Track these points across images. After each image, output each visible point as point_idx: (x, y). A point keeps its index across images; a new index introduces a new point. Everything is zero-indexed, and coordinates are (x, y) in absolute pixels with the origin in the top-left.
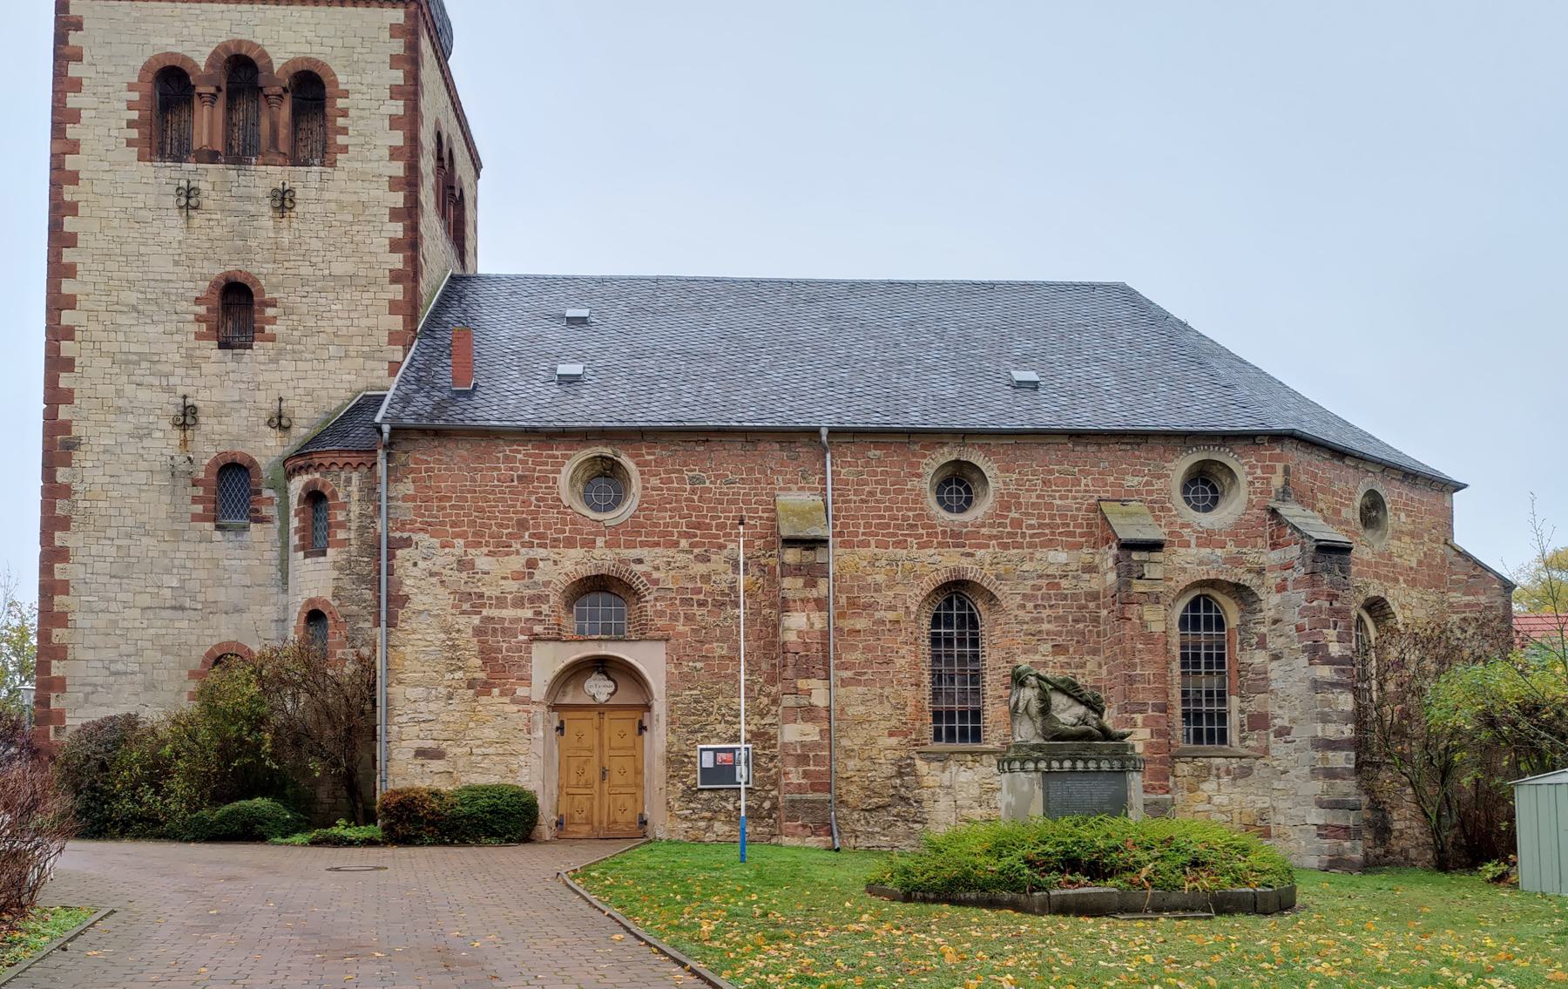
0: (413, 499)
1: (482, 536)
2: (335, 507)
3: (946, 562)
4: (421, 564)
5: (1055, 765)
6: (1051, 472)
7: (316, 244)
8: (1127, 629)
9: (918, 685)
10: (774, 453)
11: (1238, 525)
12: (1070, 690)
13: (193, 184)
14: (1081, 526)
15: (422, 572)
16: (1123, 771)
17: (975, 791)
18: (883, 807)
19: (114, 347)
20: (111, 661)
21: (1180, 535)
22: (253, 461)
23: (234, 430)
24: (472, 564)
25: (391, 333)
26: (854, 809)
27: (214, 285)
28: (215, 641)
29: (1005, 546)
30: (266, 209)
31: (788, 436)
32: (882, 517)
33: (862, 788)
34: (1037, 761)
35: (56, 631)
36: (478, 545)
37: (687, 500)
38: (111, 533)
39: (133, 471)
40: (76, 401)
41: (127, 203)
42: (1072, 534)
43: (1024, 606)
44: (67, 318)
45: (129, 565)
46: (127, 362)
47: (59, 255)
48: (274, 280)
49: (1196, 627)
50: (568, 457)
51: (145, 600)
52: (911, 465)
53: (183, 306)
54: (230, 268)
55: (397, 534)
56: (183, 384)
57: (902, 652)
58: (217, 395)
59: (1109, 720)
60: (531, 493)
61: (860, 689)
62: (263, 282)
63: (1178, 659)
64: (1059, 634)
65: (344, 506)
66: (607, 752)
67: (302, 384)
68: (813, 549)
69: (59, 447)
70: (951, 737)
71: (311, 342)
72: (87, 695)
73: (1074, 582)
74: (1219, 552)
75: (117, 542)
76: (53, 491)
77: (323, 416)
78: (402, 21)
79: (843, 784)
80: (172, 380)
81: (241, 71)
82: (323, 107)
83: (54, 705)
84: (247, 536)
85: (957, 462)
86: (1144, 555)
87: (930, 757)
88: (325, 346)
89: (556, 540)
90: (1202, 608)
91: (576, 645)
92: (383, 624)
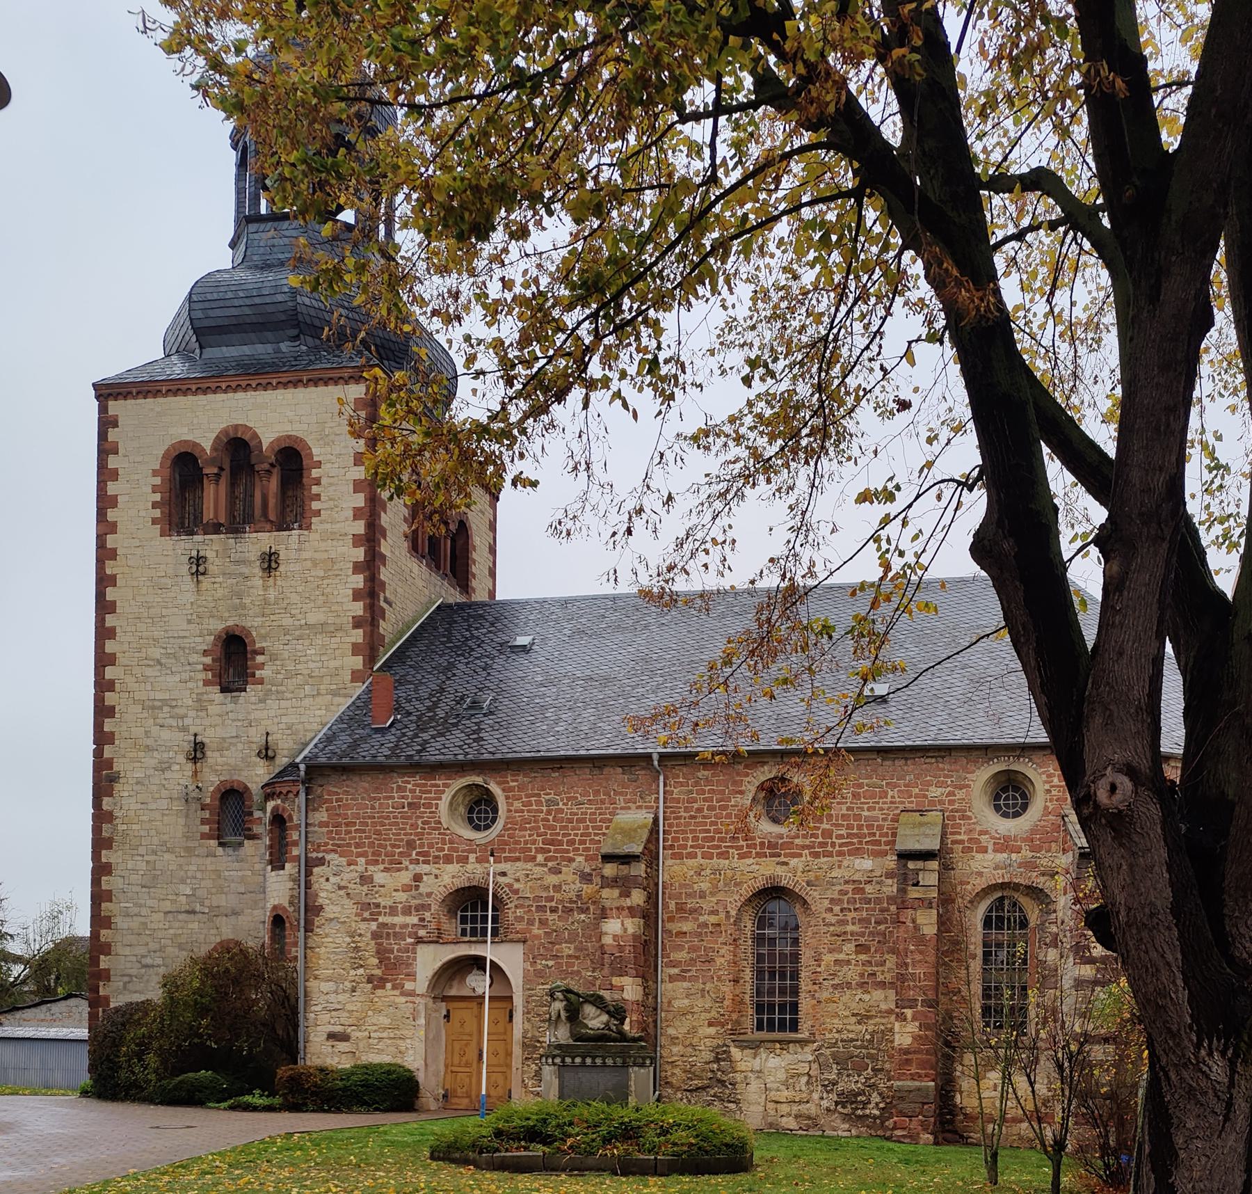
0: (326, 824)
1: (379, 855)
3: (762, 870)
4: (332, 879)
5: (568, 1060)
6: (861, 786)
7: (295, 598)
8: (901, 933)
9: (736, 981)
11: (1033, 831)
13: (201, 554)
15: (330, 885)
16: (625, 1066)
17: (782, 1076)
18: (704, 1088)
20: (143, 956)
21: (978, 841)
22: (246, 788)
23: (232, 761)
25: (353, 672)
26: (678, 1089)
27: (218, 638)
29: (816, 855)
30: (257, 571)
32: (708, 831)
33: (685, 1071)
34: (554, 1057)
35: (103, 932)
36: (376, 862)
37: (543, 820)
39: (159, 801)
40: (117, 742)
42: (878, 843)
43: (831, 910)
45: (155, 877)
47: (103, 620)
48: (263, 631)
51: (167, 906)
52: (735, 783)
53: (195, 658)
54: (230, 623)
55: (314, 855)
57: (722, 952)
58: (220, 732)
60: (418, 817)
61: (686, 984)
62: (254, 634)
64: (863, 934)
67: (284, 719)
68: (628, 863)
69: (105, 780)
70: (771, 1028)
72: (125, 984)
73: (878, 887)
74: (1014, 856)
75: (146, 858)
76: (101, 817)
79: (668, 1067)
80: (187, 721)
81: (238, 447)
82: (301, 476)
86: (920, 864)
87: (743, 1045)
88: (301, 686)
90: (1008, 907)
91: (452, 946)
92: (302, 930)
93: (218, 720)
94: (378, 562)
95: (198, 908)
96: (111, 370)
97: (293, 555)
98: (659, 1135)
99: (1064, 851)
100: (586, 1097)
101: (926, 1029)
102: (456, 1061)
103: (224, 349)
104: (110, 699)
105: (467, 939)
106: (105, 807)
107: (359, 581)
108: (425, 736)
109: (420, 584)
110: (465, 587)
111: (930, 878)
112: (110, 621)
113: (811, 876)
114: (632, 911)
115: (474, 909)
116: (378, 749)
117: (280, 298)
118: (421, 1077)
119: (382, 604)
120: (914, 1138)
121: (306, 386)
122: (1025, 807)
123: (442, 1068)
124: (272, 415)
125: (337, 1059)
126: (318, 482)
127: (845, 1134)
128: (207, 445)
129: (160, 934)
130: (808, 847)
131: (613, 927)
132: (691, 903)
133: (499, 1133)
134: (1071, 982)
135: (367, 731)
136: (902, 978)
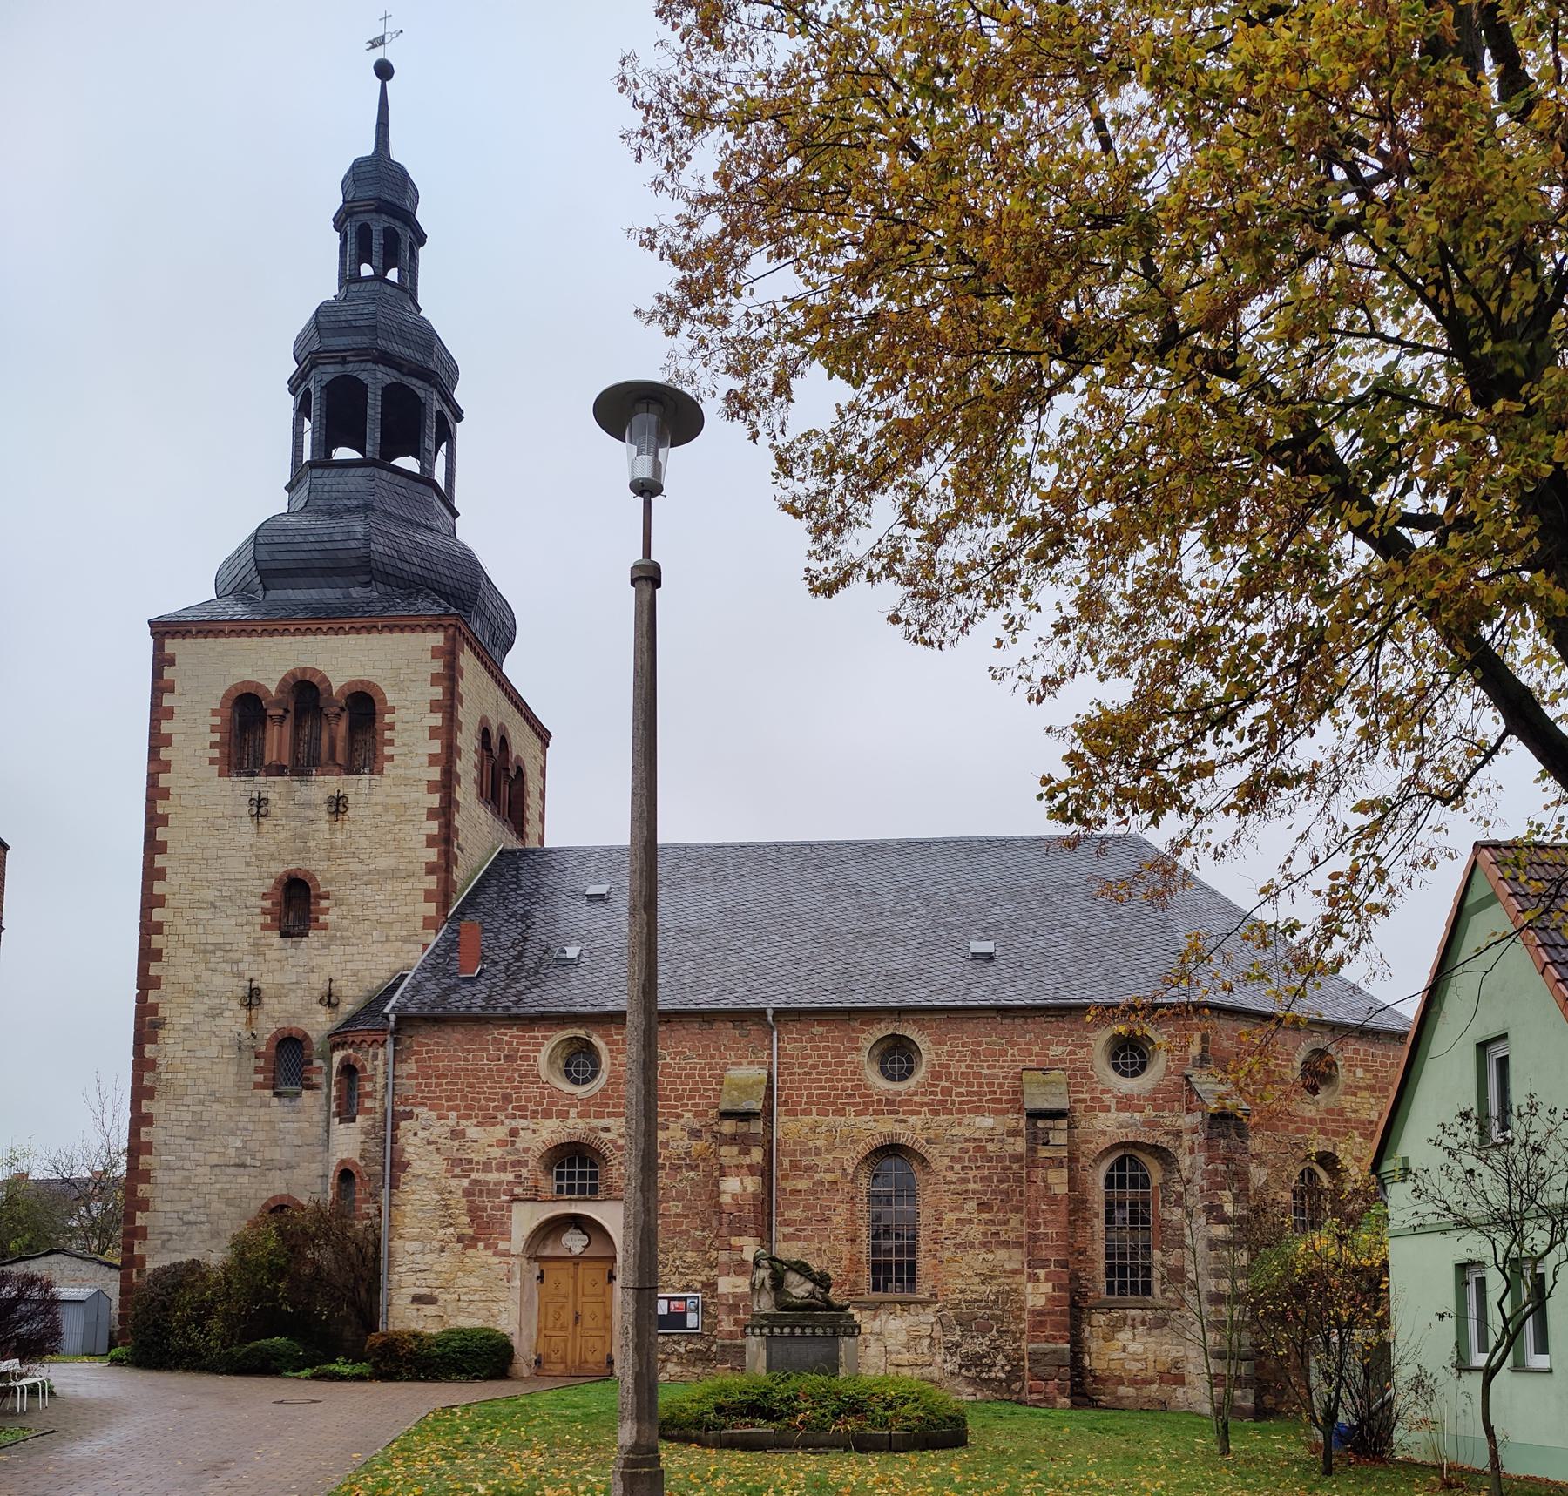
2: (365, 1079)
3: (881, 1127)
4: (421, 1134)
5: (777, 1330)
6: (980, 1044)
7: (364, 843)
9: (853, 1240)
10: (727, 1030)
11: (1156, 1090)
12: (802, 1269)
14: (1007, 1093)
15: (421, 1142)
16: (835, 1336)
17: (903, 1338)
21: (1100, 1100)
22: (306, 1035)
23: (291, 1008)
24: (463, 1134)
25: (425, 919)
27: (278, 881)
28: (270, 1195)
29: (935, 1113)
30: (324, 815)
32: (823, 1088)
34: (761, 1328)
35: (141, 1187)
36: (469, 1116)
38: (188, 1100)
39: (207, 1047)
42: (999, 1101)
43: (951, 1168)
44: (158, 915)
46: (205, 952)
47: (153, 860)
49: (1122, 1185)
52: (851, 1039)
53: (253, 901)
55: (401, 1108)
57: (839, 1210)
58: (279, 978)
60: (515, 1070)
61: (800, 1244)
63: (1102, 1216)
65: (371, 1078)
66: (581, 1299)
67: (349, 966)
69: (147, 1026)
71: (358, 929)
72: (163, 1242)
74: (1137, 1115)
76: (142, 1065)
81: (305, 692)
82: (373, 721)
84: (299, 1102)
85: (893, 1035)
86: (1049, 1123)
90: (1129, 1165)
91: (551, 1205)
93: (277, 966)
95: (249, 1161)
96: (168, 606)
97: (362, 799)
99: (1189, 1110)
100: (803, 1368)
104: (157, 941)
106: (147, 1055)
108: (519, 986)
109: (486, 829)
110: (520, 832)
111: (1060, 1138)
113: (931, 1134)
114: (752, 1169)
116: (474, 999)
117: (353, 544)
118: (515, 1342)
119: (456, 850)
120: (1050, 1402)
121: (380, 632)
122: (1143, 1067)
123: (535, 1333)
124: (343, 659)
125: (422, 1324)
127: (971, 1398)
128: (272, 687)
129: (205, 1189)
130: (926, 1104)
131: (731, 1185)
132: (806, 1161)
133: (719, 1409)
135: (454, 980)
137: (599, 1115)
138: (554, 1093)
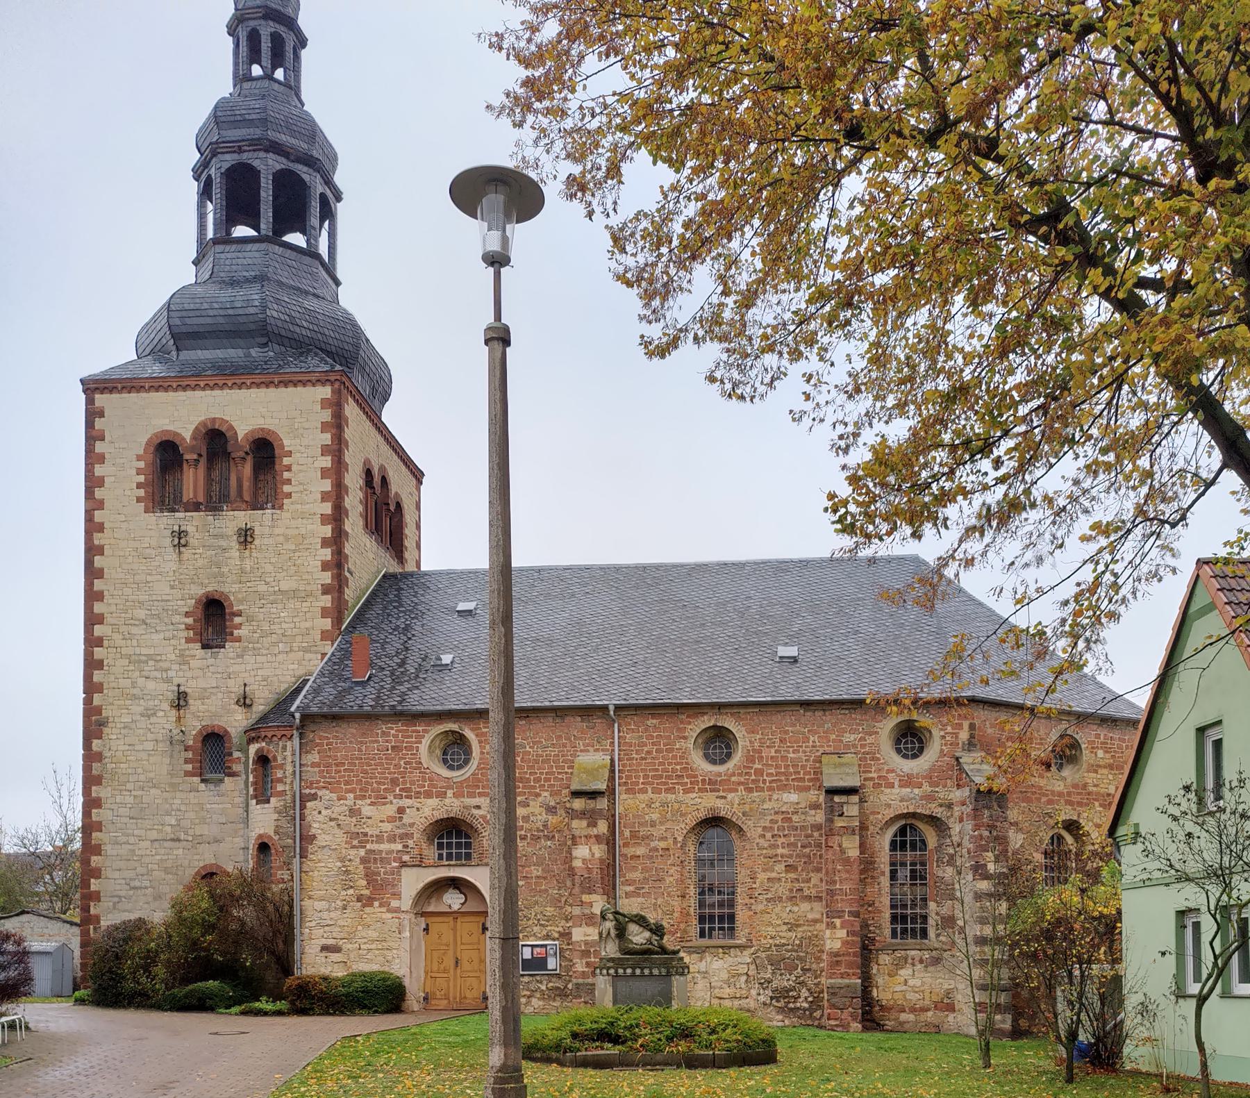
0: (318, 765)
3: (706, 803)
4: (324, 812)
5: (621, 971)
7: (269, 568)
10: (577, 723)
11: (932, 770)
12: (641, 920)
13: (183, 528)
15: (324, 818)
16: (669, 975)
17: (725, 976)
19: (130, 651)
21: (885, 778)
22: (226, 731)
23: (213, 709)
27: (198, 601)
29: (750, 790)
31: (587, 712)
32: (657, 770)
34: (608, 969)
35: (94, 858)
41: (136, 544)
42: (802, 780)
45: (142, 809)
50: (425, 731)
51: (154, 835)
52: (679, 730)
54: (210, 589)
55: (307, 791)
56: (178, 676)
58: (202, 683)
59: (668, 942)
60: (401, 759)
61: (640, 900)
63: (888, 874)
64: (790, 856)
65: (282, 766)
66: (459, 947)
72: (114, 904)
73: (803, 817)
74: (916, 791)
76: (90, 757)
77: (276, 696)
78: (329, 396)
80: (171, 674)
81: (215, 440)
82: (273, 463)
83: (92, 911)
84: (223, 787)
85: (714, 727)
86: (843, 798)
87: (692, 950)
89: (419, 793)
90: (907, 833)
91: (433, 869)
93: (200, 673)
94: (344, 539)
98: (710, 1034)
99: (959, 786)
100: (641, 1001)
101: (853, 935)
102: (435, 968)
103: (199, 352)
105: (453, 863)
107: (327, 554)
109: (371, 556)
110: (400, 558)
112: (98, 585)
115: (449, 837)
116: (365, 699)
117: (252, 310)
119: (347, 574)
121: (277, 386)
124: (246, 410)
125: (330, 969)
126: (289, 469)
127: (780, 1024)
129: (147, 860)
131: (582, 852)
132: (643, 831)
134: (971, 895)
135: (348, 684)
136: (831, 893)
137: (471, 795)
138: (433, 778)
